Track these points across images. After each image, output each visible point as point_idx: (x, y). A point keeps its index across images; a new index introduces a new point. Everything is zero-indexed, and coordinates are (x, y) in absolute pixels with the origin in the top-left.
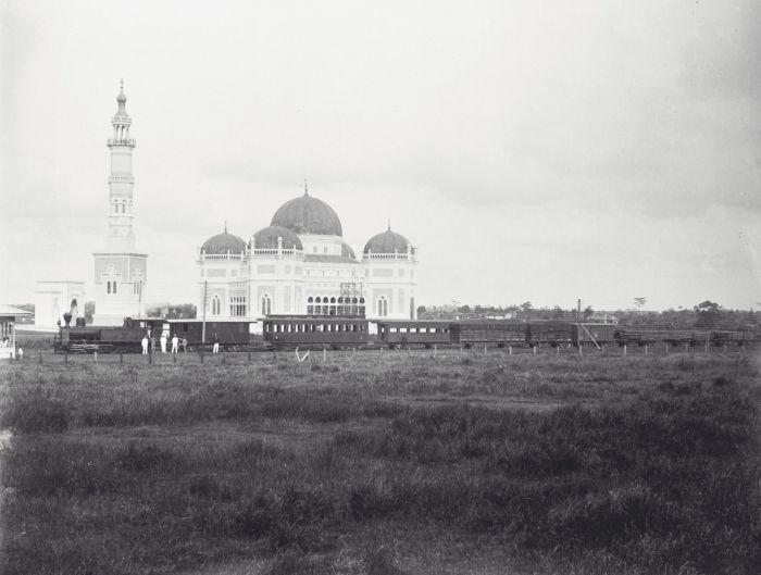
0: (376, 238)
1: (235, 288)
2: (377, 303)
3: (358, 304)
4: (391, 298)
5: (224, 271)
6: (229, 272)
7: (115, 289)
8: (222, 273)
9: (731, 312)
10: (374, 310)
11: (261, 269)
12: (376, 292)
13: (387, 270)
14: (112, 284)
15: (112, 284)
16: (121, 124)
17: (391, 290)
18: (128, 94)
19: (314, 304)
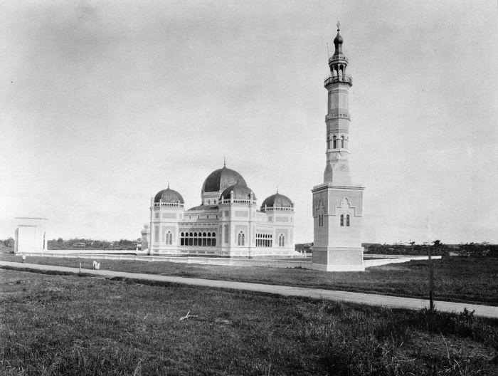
0: (266, 200)
1: (181, 227)
2: (237, 236)
3: (211, 237)
4: (287, 235)
5: (175, 214)
6: (178, 216)
7: (342, 220)
8: (173, 216)
9: (466, 245)
10: (163, 241)
11: (166, 216)
12: (278, 231)
13: (285, 218)
14: (345, 217)
15: (345, 217)
16: (335, 65)
17: (287, 230)
18: (343, 36)
19: (185, 237)
